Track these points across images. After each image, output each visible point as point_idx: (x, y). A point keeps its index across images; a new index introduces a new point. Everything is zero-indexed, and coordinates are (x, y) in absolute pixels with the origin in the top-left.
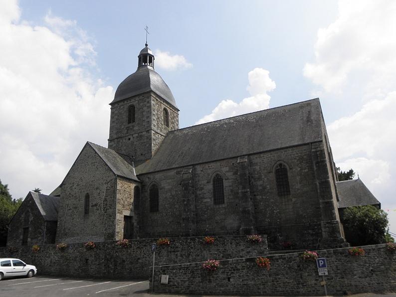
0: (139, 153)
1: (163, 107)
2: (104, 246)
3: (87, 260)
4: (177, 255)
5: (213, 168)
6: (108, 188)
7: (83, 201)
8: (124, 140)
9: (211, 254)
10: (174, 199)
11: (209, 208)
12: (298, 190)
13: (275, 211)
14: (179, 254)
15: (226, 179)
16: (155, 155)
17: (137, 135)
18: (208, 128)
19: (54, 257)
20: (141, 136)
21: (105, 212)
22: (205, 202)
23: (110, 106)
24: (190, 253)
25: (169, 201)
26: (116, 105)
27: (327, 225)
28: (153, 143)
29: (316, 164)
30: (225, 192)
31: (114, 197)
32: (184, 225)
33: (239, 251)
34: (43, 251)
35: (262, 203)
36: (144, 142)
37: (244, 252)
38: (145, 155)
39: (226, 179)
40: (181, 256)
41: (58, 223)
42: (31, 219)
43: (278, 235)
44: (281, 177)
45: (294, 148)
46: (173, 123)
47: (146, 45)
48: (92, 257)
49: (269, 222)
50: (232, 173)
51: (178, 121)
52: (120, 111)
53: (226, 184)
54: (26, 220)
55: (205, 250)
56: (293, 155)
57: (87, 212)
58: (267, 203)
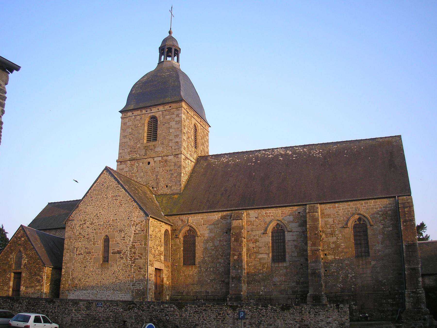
0: (162, 184)
1: (194, 121)
2: (148, 307)
3: (125, 322)
4: (245, 323)
5: (272, 216)
6: (137, 232)
7: (100, 244)
8: (141, 164)
9: (286, 324)
10: (217, 250)
11: (266, 266)
12: (379, 251)
13: (349, 275)
14: (247, 322)
15: (288, 231)
16: (184, 189)
17: (160, 159)
18: (257, 158)
19: (75, 315)
20: (166, 161)
21: (134, 263)
22: (260, 259)
23: (120, 115)
24: (262, 321)
25: (210, 253)
26: (130, 114)
27: (412, 294)
28: (183, 171)
29: (403, 223)
30: (286, 247)
31: (145, 244)
32: (233, 285)
33: (318, 322)
34: (59, 306)
35: (334, 265)
36: (171, 170)
37: (323, 323)
38: (171, 187)
39: (288, 231)
40: (251, 324)
41: (63, 270)
42: (25, 261)
43: (352, 303)
44: (358, 234)
45: (376, 200)
46: (203, 144)
47: (170, 32)
48: (132, 319)
49: (340, 287)
50: (297, 224)
51: (208, 141)
52: (137, 122)
53: (288, 237)
54: (19, 263)
55: (278, 318)
56: (376, 208)
57: (106, 259)
58: (341, 265)
